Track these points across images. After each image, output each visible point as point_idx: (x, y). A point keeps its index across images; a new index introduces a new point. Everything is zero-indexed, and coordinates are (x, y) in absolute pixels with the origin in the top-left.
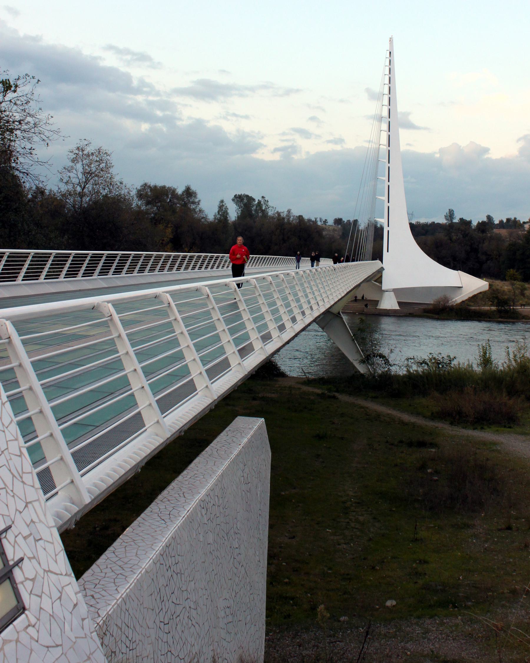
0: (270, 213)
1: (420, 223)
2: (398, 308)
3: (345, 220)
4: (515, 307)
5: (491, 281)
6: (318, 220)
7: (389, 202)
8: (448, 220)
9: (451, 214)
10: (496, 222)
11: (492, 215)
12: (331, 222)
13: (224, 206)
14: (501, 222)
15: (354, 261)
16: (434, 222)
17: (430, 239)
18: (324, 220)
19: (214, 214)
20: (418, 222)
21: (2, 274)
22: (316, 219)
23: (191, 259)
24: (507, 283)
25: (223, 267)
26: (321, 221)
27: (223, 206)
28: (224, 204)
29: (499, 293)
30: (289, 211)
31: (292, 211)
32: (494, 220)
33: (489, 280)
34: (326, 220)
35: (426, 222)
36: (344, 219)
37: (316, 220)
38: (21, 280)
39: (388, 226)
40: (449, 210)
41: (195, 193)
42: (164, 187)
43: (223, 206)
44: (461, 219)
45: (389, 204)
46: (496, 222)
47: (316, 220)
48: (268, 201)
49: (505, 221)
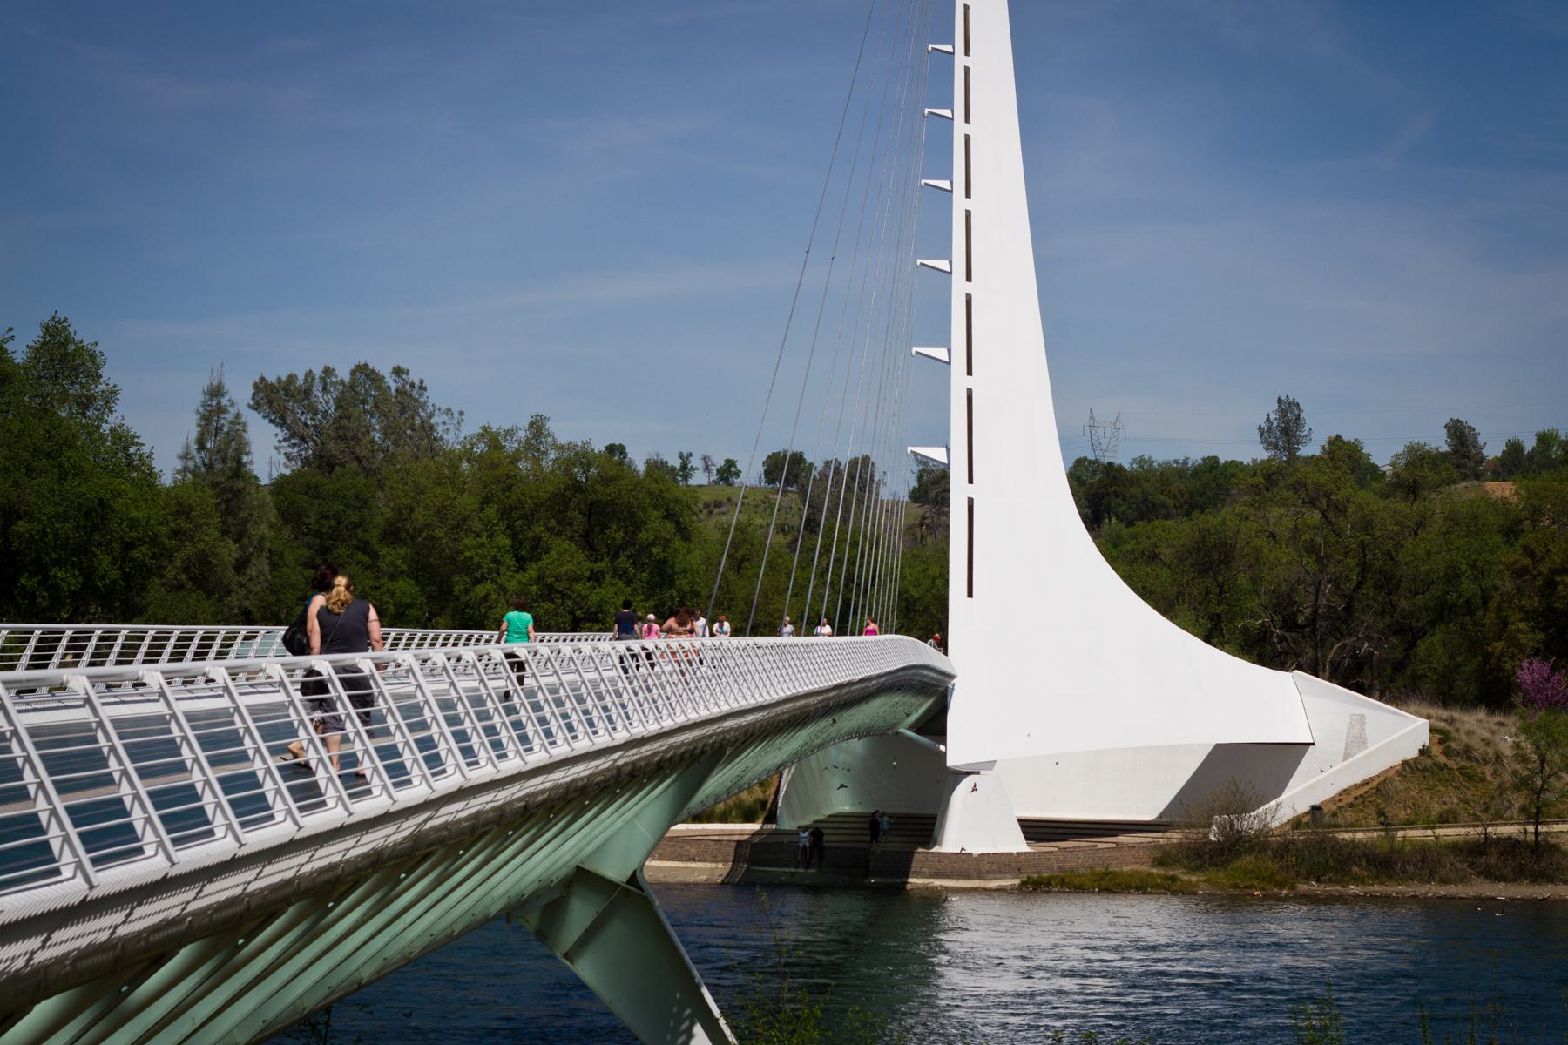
0: (453, 436)
1: (1151, 462)
2: (1526, 453)
3: (815, 458)
4: (1543, 829)
5: (1445, 714)
6: (696, 462)
7: (969, 372)
8: (1276, 447)
9: (1287, 422)
10: (1493, 449)
11: (1470, 420)
12: (751, 473)
13: (226, 412)
14: (1514, 448)
15: (845, 634)
16: (1215, 460)
17: (1175, 533)
18: (721, 463)
19: (180, 451)
20: (1141, 461)
21: (4, 649)
22: (685, 459)
23: (129, 647)
24: (1512, 722)
25: (432, 645)
26: (707, 469)
27: (221, 410)
28: (224, 401)
29: (1474, 447)
30: (538, 427)
31: (551, 426)
32: (1481, 441)
33: (1433, 711)
34: (730, 463)
35: (1181, 459)
36: (809, 458)
37: (684, 467)
38: (25, 665)
39: (971, 481)
40: (1280, 401)
41: (93, 357)
42: (1212, 463)
43: (221, 410)
44: (1336, 442)
45: (970, 382)
46: (1493, 449)
47: (684, 467)
48: (422, 388)
49: (1529, 444)
